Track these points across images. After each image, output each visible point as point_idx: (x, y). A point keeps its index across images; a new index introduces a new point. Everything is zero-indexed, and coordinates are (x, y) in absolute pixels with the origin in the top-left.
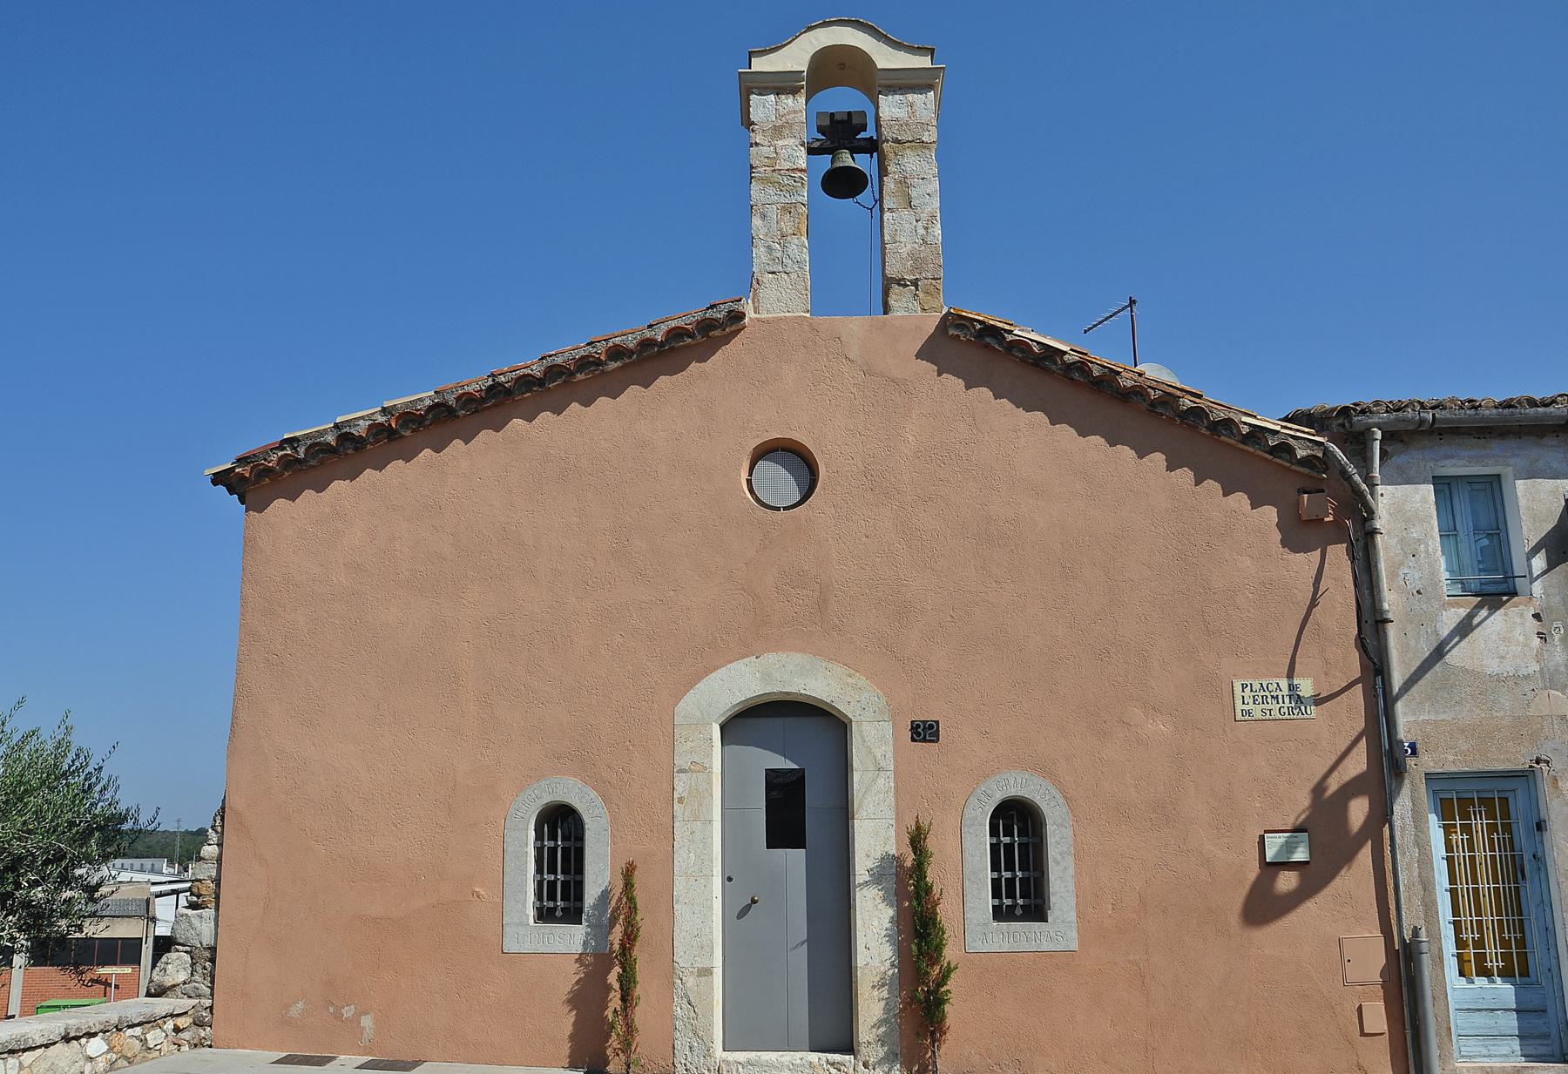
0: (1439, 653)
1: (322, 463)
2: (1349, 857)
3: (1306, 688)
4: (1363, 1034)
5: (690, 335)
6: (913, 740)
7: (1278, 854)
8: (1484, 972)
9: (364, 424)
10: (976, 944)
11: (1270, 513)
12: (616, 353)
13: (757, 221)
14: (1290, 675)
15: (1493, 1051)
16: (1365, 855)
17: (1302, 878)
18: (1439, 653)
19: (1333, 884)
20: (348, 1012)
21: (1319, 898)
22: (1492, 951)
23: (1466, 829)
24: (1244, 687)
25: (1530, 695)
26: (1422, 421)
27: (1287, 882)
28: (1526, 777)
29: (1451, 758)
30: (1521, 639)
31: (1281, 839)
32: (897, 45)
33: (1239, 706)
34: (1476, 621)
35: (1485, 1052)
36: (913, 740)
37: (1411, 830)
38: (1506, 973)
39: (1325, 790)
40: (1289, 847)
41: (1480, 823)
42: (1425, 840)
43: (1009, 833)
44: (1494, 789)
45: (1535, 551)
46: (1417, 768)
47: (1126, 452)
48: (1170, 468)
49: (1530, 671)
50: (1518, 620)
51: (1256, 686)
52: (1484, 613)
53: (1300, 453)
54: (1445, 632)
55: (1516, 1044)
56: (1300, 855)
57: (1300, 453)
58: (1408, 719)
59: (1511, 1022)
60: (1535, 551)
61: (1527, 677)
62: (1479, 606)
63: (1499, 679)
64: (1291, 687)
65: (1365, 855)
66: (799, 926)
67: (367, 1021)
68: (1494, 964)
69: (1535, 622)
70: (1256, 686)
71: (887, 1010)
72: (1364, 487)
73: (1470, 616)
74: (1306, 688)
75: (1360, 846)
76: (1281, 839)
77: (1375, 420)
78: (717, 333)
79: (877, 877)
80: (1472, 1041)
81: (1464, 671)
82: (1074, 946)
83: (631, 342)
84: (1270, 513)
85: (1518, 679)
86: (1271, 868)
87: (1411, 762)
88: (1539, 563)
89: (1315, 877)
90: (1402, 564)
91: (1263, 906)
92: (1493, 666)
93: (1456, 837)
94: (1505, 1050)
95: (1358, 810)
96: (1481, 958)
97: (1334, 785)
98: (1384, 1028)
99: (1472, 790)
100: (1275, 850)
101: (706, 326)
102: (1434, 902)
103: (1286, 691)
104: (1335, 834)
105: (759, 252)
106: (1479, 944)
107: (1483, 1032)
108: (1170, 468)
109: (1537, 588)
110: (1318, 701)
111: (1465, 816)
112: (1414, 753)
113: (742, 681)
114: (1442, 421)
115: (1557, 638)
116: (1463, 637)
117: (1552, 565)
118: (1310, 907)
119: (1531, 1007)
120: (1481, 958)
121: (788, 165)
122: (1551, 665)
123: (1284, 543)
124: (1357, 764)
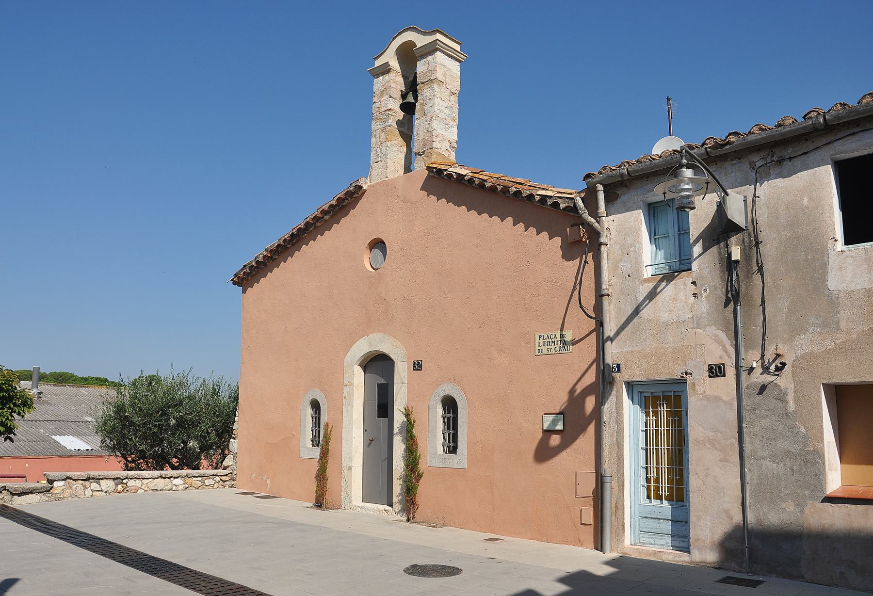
0: (637, 311)
1: (258, 273)
2: (584, 429)
3: (568, 337)
4: (582, 524)
5: (343, 200)
6: (710, 376)
7: (549, 426)
8: (659, 497)
9: (261, 256)
10: (433, 464)
11: (558, 240)
12: (324, 212)
13: (373, 140)
14: (562, 330)
15: (657, 541)
16: (592, 428)
17: (562, 439)
18: (637, 311)
19: (575, 443)
20: (265, 477)
21: (569, 450)
22: (665, 485)
23: (656, 414)
24: (540, 337)
25: (685, 333)
26: (622, 175)
27: (555, 440)
28: (682, 382)
29: (638, 373)
30: (683, 298)
31: (551, 418)
32: (424, 33)
33: (537, 348)
34: (659, 289)
35: (652, 542)
36: (710, 376)
37: (614, 414)
38: (669, 498)
39: (575, 391)
40: (554, 422)
41: (663, 410)
42: (629, 420)
43: (449, 413)
44: (670, 390)
45: (696, 241)
46: (621, 378)
47: (496, 219)
48: (514, 225)
49: (687, 317)
50: (682, 287)
51: (546, 337)
52: (664, 284)
53: (562, 206)
54: (641, 299)
55: (669, 540)
56: (560, 427)
57: (562, 206)
58: (613, 353)
59: (667, 527)
60: (696, 241)
61: (683, 322)
62: (661, 281)
63: (667, 324)
64: (562, 336)
65: (592, 428)
66: (853, 506)
67: (269, 481)
68: (665, 493)
69: (693, 287)
70: (546, 337)
71: (402, 489)
72: (592, 220)
73: (656, 287)
74: (568, 337)
75: (591, 422)
76: (551, 418)
77: (597, 179)
78: (355, 195)
79: (400, 432)
80: (646, 535)
81: (649, 321)
82: (466, 467)
83: (326, 207)
84: (558, 240)
85: (679, 323)
86: (548, 432)
87: (617, 375)
88: (697, 249)
89: (569, 436)
90: (621, 260)
91: (544, 453)
92: (665, 317)
93: (652, 418)
94: (663, 542)
95: (590, 403)
96: (657, 489)
97: (579, 389)
98: (592, 522)
99: (659, 390)
100: (548, 423)
101: (349, 194)
102: (622, 456)
103: (559, 338)
104: (578, 418)
105: (373, 154)
106: (657, 480)
107: (652, 530)
108: (514, 225)
109: (695, 266)
110: (574, 343)
111: (655, 406)
112: (619, 370)
113: (362, 347)
114: (634, 171)
115: (704, 295)
116: (651, 300)
117: (705, 249)
118: (564, 454)
119: (679, 519)
120: (657, 489)
121: (384, 109)
122: (699, 313)
123: (563, 257)
124: (590, 378)
